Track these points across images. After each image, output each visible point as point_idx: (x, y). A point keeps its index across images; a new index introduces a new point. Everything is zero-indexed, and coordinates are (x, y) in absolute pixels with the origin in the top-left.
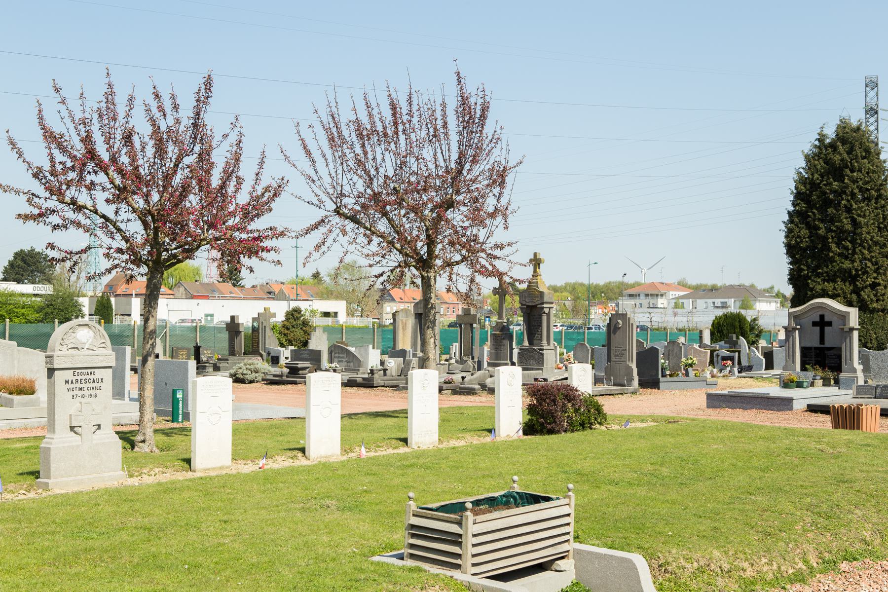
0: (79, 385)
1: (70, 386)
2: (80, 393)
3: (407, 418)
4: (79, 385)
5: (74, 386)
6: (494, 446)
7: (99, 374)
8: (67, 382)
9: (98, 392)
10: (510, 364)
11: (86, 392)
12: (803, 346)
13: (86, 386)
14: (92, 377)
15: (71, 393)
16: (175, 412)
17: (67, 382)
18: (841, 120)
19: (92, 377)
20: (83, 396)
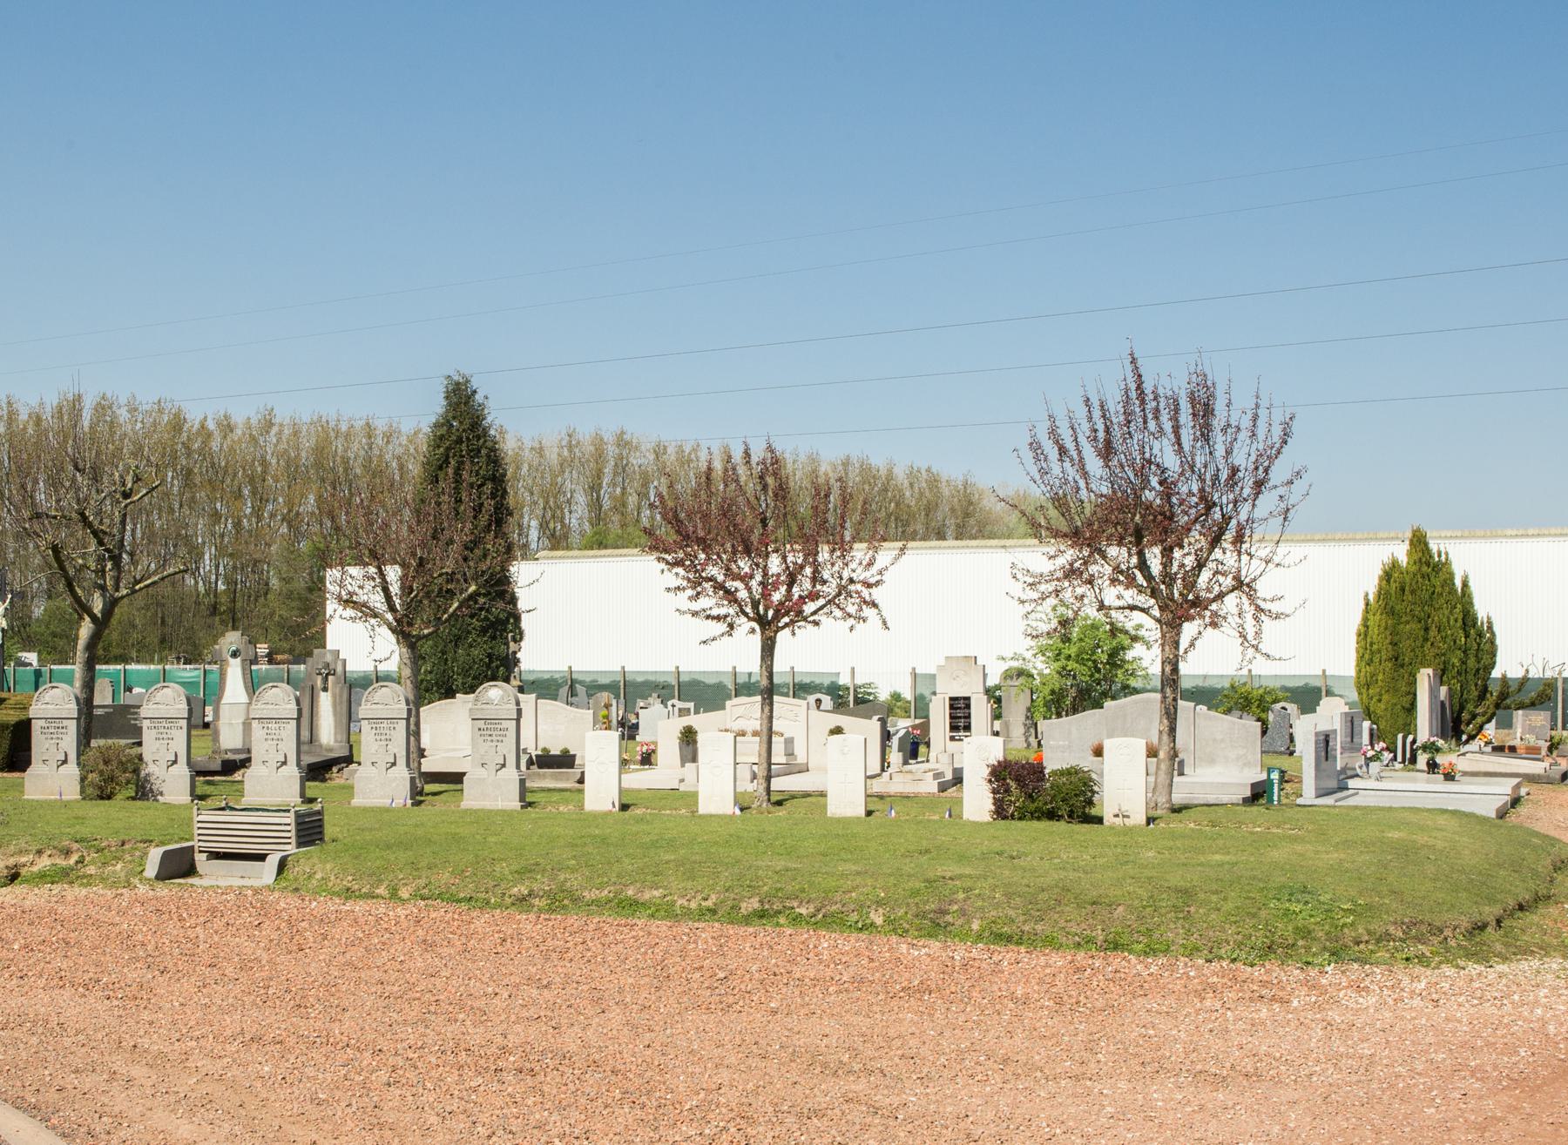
0: (489, 732)
1: (482, 732)
2: (489, 738)
3: (462, 790)
4: (489, 732)
5: (485, 733)
6: (161, 411)
7: (505, 724)
8: (480, 729)
9: (504, 739)
10: (877, 786)
11: (494, 738)
12: (1100, 758)
13: (494, 733)
14: (499, 726)
15: (483, 738)
16: (345, 721)
17: (480, 729)
18: (225, 416)
19: (499, 726)
20: (492, 741)
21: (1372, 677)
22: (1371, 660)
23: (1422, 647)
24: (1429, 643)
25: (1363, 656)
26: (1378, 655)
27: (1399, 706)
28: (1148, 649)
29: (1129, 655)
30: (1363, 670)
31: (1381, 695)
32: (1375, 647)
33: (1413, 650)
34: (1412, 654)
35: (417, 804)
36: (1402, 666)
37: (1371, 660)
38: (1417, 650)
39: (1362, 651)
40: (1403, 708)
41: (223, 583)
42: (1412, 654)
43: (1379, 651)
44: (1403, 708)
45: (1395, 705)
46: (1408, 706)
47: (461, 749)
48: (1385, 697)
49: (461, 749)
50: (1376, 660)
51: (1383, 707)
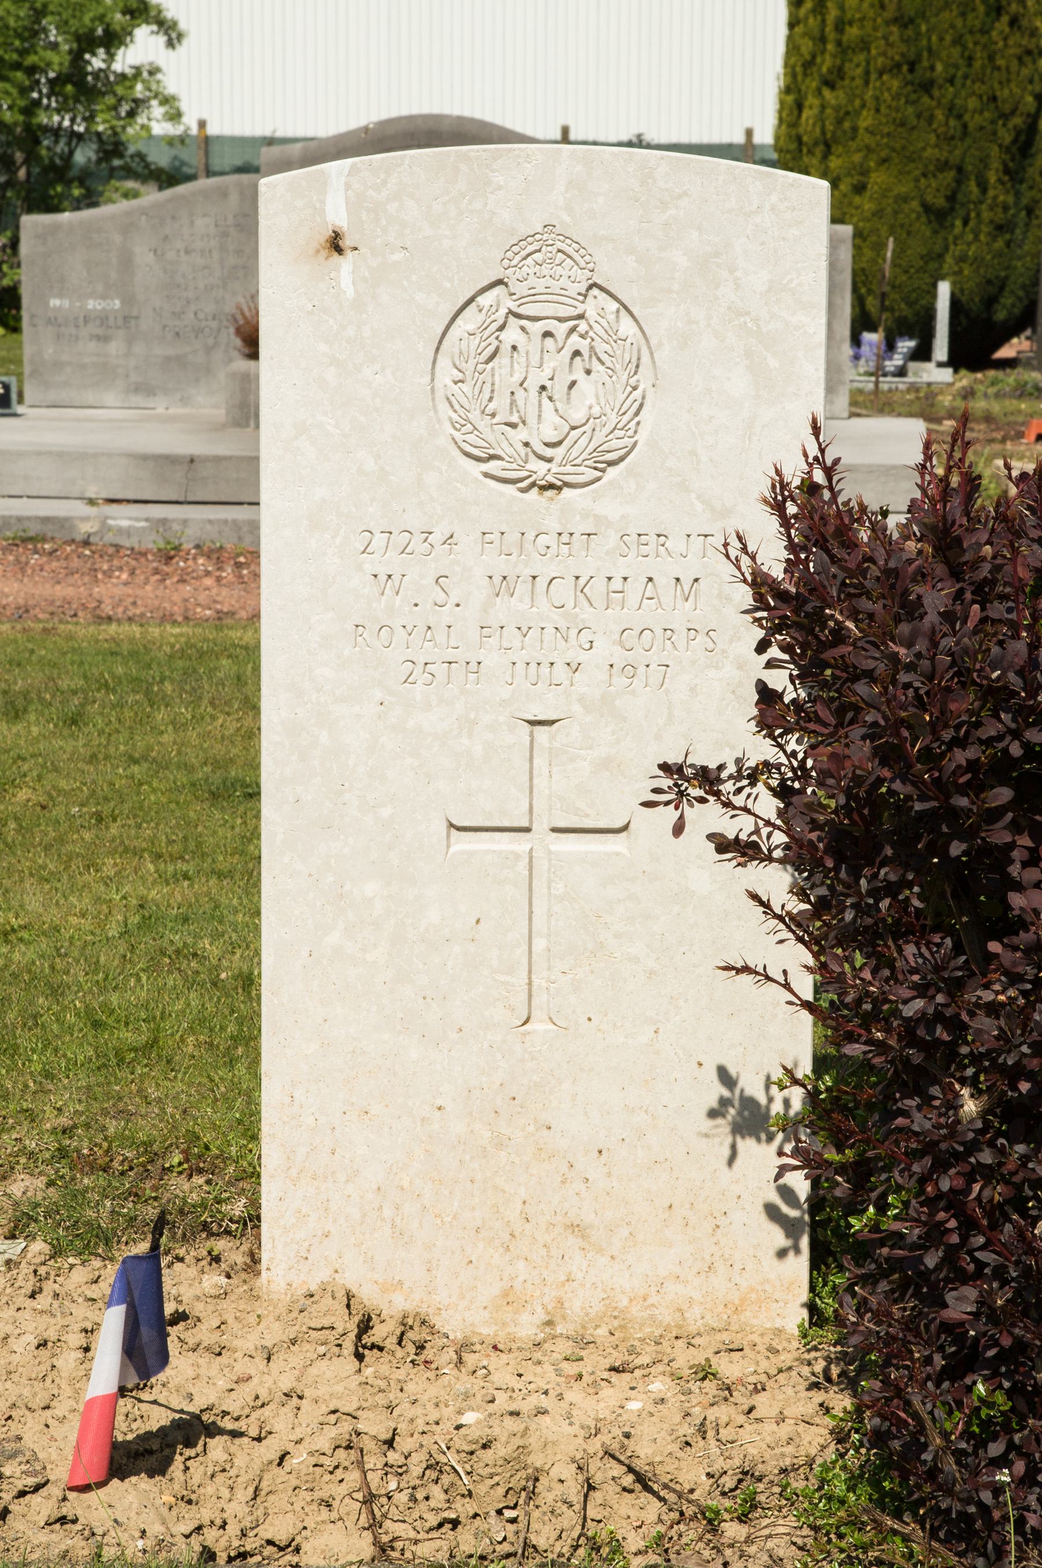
21: (839, 122)
22: (839, 72)
23: (984, 31)
24: (1005, 19)
25: (808, 65)
26: (861, 57)
27: (915, 204)
28: (170, 44)
29: (125, 60)
30: (811, 100)
31: (865, 172)
32: (853, 32)
33: (958, 41)
34: (956, 51)
35: (81, 5)
36: (927, 87)
37: (839, 72)
38: (969, 40)
39: (807, 46)
40: (927, 208)
41: (1021, 1439)
42: (956, 51)
43: (864, 45)
44: (927, 208)
45: (905, 199)
46: (940, 202)
47: (639, 351)
48: (878, 179)
49: (639, 351)
50: (855, 70)
51: (868, 206)
